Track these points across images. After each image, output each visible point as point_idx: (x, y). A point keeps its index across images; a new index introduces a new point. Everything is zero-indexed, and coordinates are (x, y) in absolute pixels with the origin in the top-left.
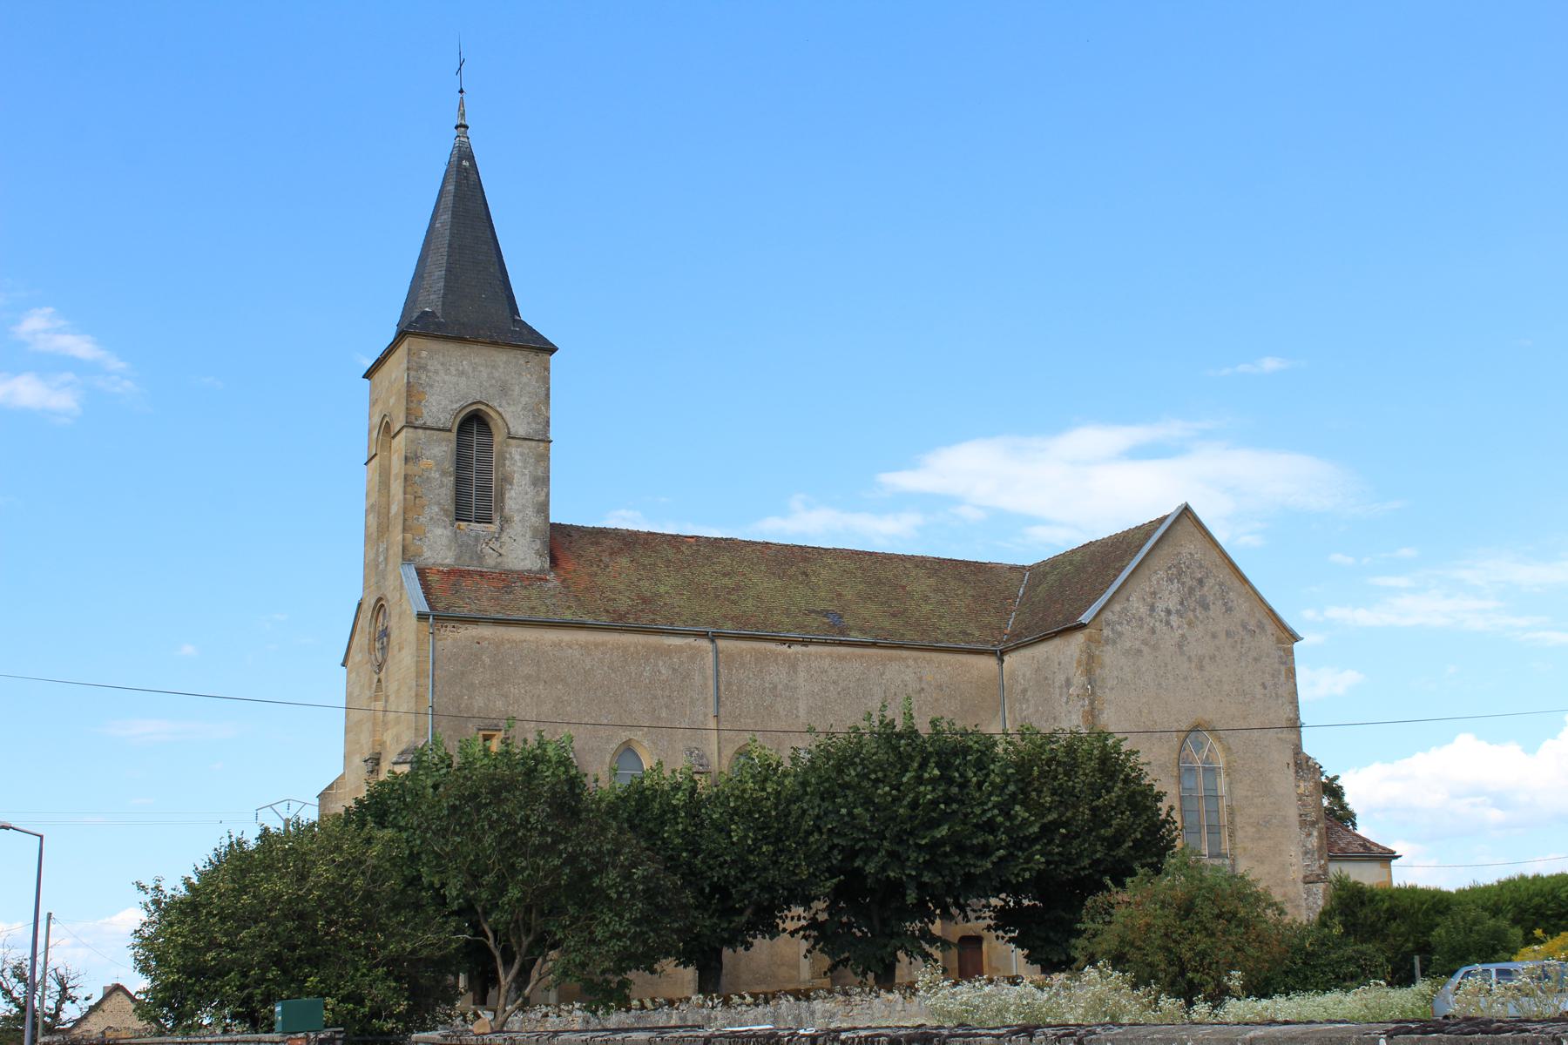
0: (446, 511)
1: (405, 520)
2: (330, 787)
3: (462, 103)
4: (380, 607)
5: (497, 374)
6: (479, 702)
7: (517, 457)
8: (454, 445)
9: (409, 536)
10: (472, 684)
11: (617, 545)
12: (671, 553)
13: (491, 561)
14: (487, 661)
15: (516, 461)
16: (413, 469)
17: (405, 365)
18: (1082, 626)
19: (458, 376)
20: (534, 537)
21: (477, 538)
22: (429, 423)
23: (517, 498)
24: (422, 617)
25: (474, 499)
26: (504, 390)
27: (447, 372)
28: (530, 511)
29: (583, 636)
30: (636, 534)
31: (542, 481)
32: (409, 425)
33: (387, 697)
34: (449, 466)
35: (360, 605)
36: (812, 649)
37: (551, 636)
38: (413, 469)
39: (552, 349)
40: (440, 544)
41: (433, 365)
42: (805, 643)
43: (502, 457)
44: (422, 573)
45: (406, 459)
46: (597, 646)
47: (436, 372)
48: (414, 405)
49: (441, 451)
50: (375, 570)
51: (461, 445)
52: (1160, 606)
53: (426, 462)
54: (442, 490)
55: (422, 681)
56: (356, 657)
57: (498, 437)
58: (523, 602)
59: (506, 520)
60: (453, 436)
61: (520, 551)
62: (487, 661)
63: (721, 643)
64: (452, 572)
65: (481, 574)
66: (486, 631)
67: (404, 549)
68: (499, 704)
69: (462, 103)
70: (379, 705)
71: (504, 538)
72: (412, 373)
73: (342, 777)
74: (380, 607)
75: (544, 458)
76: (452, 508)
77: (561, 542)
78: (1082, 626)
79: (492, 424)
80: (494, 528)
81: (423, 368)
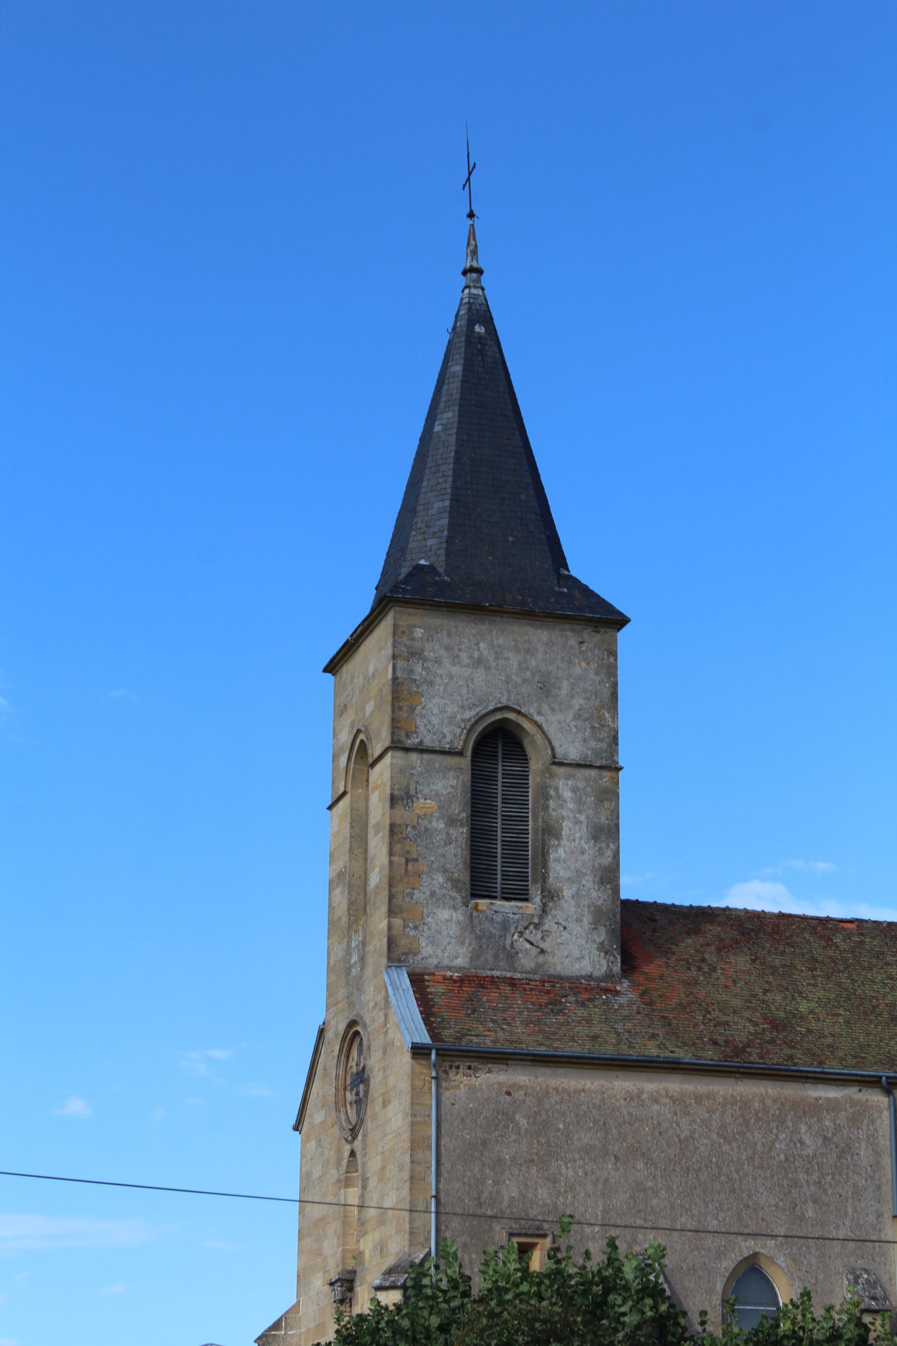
3: (472, 234)
4: (352, 1036)
6: (510, 1190)
7: (567, 794)
8: (467, 777)
9: (398, 922)
10: (500, 1161)
13: (527, 961)
15: (566, 801)
17: (388, 651)
19: (473, 669)
23: (568, 859)
24: (418, 1051)
25: (499, 858)
28: (588, 882)
29: (675, 1085)
31: (607, 832)
33: (365, 1180)
34: (460, 810)
37: (623, 1085)
38: (402, 815)
39: (620, 621)
40: (446, 937)
44: (418, 981)
46: (699, 1099)
47: (438, 661)
48: (403, 714)
49: (445, 787)
54: (450, 848)
56: (317, 1116)
57: (536, 764)
58: (580, 1030)
59: (550, 896)
60: (466, 762)
61: (575, 947)
65: (512, 983)
66: (522, 1077)
68: (543, 1193)
69: (472, 234)
70: (352, 1195)
71: (549, 924)
74: (352, 1036)
75: (611, 794)
76: (465, 877)
77: (642, 931)
80: (531, 908)
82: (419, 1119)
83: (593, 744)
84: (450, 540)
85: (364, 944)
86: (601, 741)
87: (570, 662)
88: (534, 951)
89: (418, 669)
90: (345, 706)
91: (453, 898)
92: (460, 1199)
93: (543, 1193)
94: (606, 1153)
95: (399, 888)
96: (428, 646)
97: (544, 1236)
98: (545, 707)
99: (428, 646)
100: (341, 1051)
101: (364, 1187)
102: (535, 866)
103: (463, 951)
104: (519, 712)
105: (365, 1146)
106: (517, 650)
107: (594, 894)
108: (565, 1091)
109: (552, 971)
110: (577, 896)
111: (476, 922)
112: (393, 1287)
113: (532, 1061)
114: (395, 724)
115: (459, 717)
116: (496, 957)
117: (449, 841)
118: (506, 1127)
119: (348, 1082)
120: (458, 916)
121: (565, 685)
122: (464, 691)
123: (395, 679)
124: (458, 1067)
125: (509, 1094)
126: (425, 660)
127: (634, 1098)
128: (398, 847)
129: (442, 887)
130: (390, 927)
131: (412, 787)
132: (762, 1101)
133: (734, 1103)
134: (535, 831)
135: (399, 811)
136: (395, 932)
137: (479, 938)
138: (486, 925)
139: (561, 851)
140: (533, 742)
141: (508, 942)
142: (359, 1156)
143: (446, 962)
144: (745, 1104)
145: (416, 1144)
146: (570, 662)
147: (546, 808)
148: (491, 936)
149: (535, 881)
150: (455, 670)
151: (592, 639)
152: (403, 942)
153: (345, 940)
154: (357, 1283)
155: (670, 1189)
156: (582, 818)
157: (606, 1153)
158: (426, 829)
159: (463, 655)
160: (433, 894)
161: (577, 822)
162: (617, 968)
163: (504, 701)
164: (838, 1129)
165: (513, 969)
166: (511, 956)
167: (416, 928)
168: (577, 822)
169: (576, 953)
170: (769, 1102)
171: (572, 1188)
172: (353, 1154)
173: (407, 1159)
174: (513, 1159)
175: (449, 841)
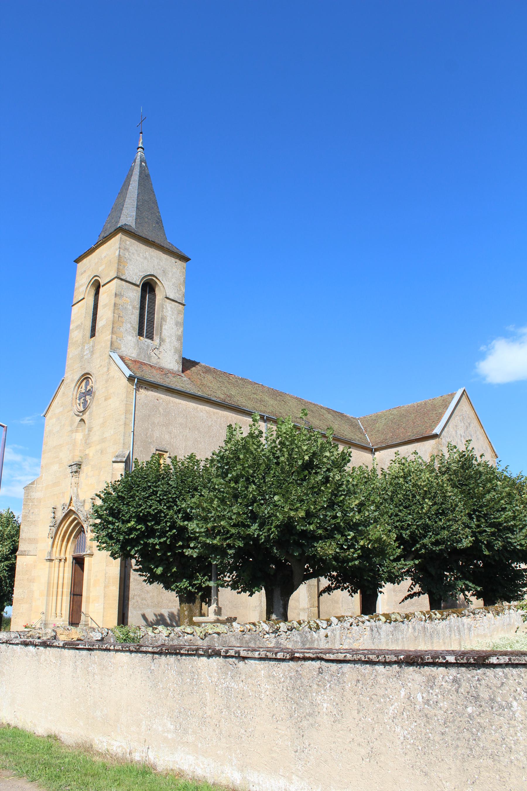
0: (134, 328)
1: (113, 328)
5: (161, 264)
6: (157, 434)
7: (169, 309)
9: (114, 337)
10: (154, 423)
13: (154, 361)
14: (162, 411)
16: (119, 301)
17: (117, 245)
18: (436, 436)
20: (175, 352)
21: (148, 346)
22: (128, 279)
24: (131, 379)
28: (174, 339)
33: (90, 430)
38: (119, 301)
40: (131, 344)
41: (132, 249)
45: (116, 295)
47: (133, 254)
48: (121, 267)
49: (135, 294)
51: (143, 298)
52: (459, 432)
59: (162, 340)
60: (139, 289)
62: (162, 411)
64: (135, 361)
65: (151, 366)
67: (112, 343)
68: (167, 437)
70: (79, 436)
71: (161, 349)
72: (121, 251)
78: (436, 436)
81: (126, 249)
82: (128, 403)
83: (177, 295)
84: (136, 219)
86: (180, 294)
87: (172, 267)
88: (157, 357)
89: (127, 254)
90: (85, 271)
91: (133, 333)
92: (140, 434)
93: (167, 437)
94: (187, 427)
95: (116, 325)
96: (130, 248)
97: (167, 452)
98: (164, 279)
99: (130, 248)
100: (76, 385)
102: (157, 329)
104: (157, 278)
106: (157, 258)
107: (175, 343)
108: (175, 402)
109: (161, 365)
110: (170, 342)
111: (139, 343)
113: (166, 390)
115: (138, 274)
116: (145, 356)
117: (132, 314)
118: (156, 411)
119: (78, 396)
121: (170, 273)
122: (140, 266)
123: (119, 255)
124: (142, 387)
125: (158, 400)
126: (129, 252)
128: (116, 311)
129: (129, 329)
130: (112, 338)
131: (122, 293)
132: (231, 418)
133: (224, 417)
134: (158, 318)
135: (118, 298)
136: (113, 340)
137: (140, 349)
138: (142, 345)
139: (166, 326)
140: (160, 289)
141: (149, 352)
143: (129, 354)
145: (127, 412)
146: (172, 267)
147: (163, 311)
148: (143, 349)
149: (157, 335)
150: (138, 258)
152: (116, 344)
153: (80, 348)
155: (205, 442)
156: (173, 317)
157: (187, 427)
158: (126, 308)
159: (141, 254)
160: (126, 330)
161: (171, 318)
162: (181, 369)
163: (152, 274)
166: (150, 357)
167: (120, 340)
168: (171, 318)
169: (169, 361)
170: (233, 419)
173: (123, 417)
174: (158, 423)
175: (132, 314)
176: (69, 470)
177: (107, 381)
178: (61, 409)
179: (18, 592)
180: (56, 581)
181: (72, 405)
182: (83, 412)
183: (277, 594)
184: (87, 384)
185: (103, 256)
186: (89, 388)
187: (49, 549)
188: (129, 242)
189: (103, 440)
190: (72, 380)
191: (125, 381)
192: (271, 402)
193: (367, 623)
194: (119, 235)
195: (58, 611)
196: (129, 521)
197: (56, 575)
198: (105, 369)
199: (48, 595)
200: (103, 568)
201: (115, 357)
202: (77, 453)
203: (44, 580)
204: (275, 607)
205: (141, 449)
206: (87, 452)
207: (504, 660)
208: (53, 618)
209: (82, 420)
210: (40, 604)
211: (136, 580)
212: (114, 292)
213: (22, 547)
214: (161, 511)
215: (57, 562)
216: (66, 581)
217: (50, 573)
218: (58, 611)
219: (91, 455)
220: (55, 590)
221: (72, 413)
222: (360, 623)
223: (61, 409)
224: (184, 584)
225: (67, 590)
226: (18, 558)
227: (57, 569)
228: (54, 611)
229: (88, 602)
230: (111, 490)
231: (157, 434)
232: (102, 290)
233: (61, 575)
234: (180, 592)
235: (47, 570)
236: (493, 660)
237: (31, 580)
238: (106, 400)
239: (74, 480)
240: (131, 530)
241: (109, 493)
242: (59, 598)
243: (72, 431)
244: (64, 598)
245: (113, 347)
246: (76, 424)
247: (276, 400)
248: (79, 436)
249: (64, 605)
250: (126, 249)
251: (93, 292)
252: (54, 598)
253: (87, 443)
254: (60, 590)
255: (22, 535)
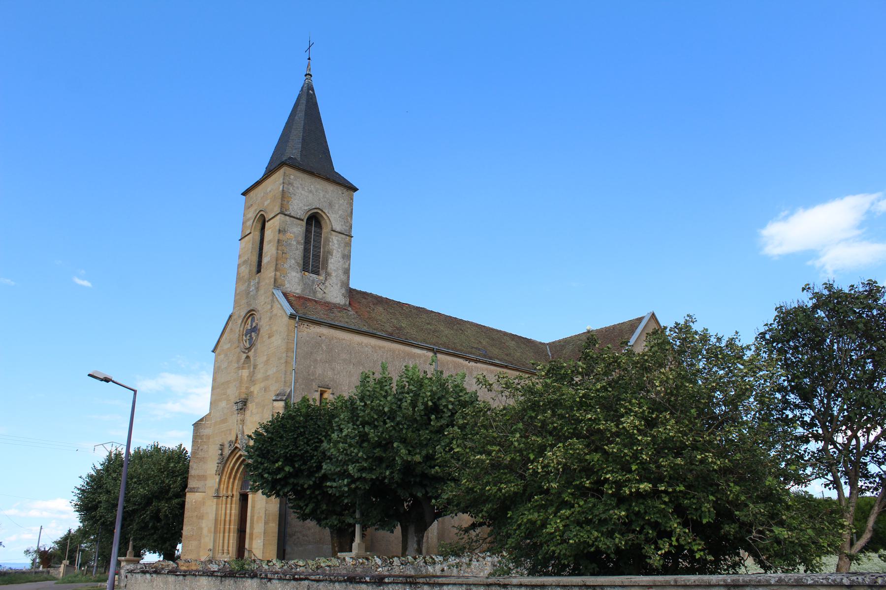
0: (298, 263)
2: (202, 420)
3: (309, 64)
4: (251, 314)
6: (319, 371)
7: (336, 242)
8: (304, 229)
9: (278, 273)
10: (316, 360)
11: (375, 301)
12: (400, 309)
13: (319, 295)
15: (335, 243)
17: (281, 180)
19: (307, 194)
21: (313, 281)
23: (334, 263)
24: (292, 317)
25: (313, 261)
26: (331, 205)
27: (303, 189)
28: (340, 272)
29: (373, 341)
30: (381, 297)
32: (282, 213)
33: (255, 367)
34: (301, 239)
35: (230, 316)
36: (479, 365)
37: (358, 338)
38: (282, 237)
39: (355, 189)
40: (294, 281)
41: (297, 184)
42: (476, 361)
43: (327, 240)
46: (380, 348)
47: (298, 188)
49: (297, 230)
50: (244, 294)
51: (308, 231)
53: (289, 235)
54: (297, 252)
55: (290, 354)
56: (225, 346)
57: (325, 230)
59: (328, 275)
60: (304, 223)
61: (335, 295)
63: (439, 356)
64: (299, 297)
65: (316, 301)
67: (275, 280)
68: (330, 373)
69: (309, 64)
70: (245, 373)
71: (327, 284)
73: (209, 414)
74: (251, 314)
75: (348, 245)
76: (301, 262)
77: (354, 295)
79: (323, 223)
80: (322, 278)
81: (290, 184)
85: (258, 283)
95: (279, 262)
101: (255, 368)
103: (299, 288)
105: (255, 356)
110: (336, 276)
112: (281, 400)
114: (282, 206)
120: (298, 275)
127: (360, 344)
142: (252, 359)
144: (394, 351)
149: (323, 269)
151: (347, 193)
154: (249, 402)
164: (420, 364)
165: (315, 297)
166: (315, 292)
171: (339, 373)
172: (248, 357)
173: (284, 355)
176: (235, 407)
177: (271, 318)
178: (229, 345)
179: (187, 530)
180: (223, 518)
181: (239, 342)
182: (249, 349)
183: (412, 530)
184: (253, 320)
185: (269, 190)
186: (254, 325)
187: (217, 486)
188: (293, 174)
189: (266, 378)
190: (239, 317)
191: (286, 319)
192: (447, 332)
193: (489, 559)
194: (282, 171)
195: (226, 548)
196: (277, 461)
197: (223, 512)
198: (269, 307)
199: (215, 532)
200: (263, 507)
201: (279, 295)
202: (243, 390)
203: (212, 516)
204: (409, 543)
205: (303, 386)
206: (252, 389)
207: (391, 580)
208: (220, 555)
209: (248, 357)
210: (208, 541)
211: (293, 517)
212: (277, 228)
213: (192, 484)
214: (307, 452)
215: (224, 498)
216: (233, 518)
217: (217, 510)
218: (226, 548)
219: (255, 392)
220: (222, 526)
221: (238, 350)
222: (481, 559)
223: (229, 345)
224: (334, 520)
225: (234, 527)
226: (188, 495)
227: (224, 506)
228: (221, 548)
229: (251, 539)
230: (261, 431)
231: (319, 371)
232: (267, 225)
233: (228, 512)
234: (331, 527)
235: (215, 506)
236: (386, 580)
237: (200, 517)
238: (269, 337)
239: (240, 417)
240: (280, 469)
241: (261, 435)
242: (227, 534)
243: (238, 368)
244: (232, 534)
245: (277, 284)
246: (242, 361)
247: (452, 329)
248: (245, 373)
249: (231, 541)
250: (290, 184)
251: (259, 226)
252: (222, 535)
253: (252, 380)
254: (227, 527)
255: (192, 472)
